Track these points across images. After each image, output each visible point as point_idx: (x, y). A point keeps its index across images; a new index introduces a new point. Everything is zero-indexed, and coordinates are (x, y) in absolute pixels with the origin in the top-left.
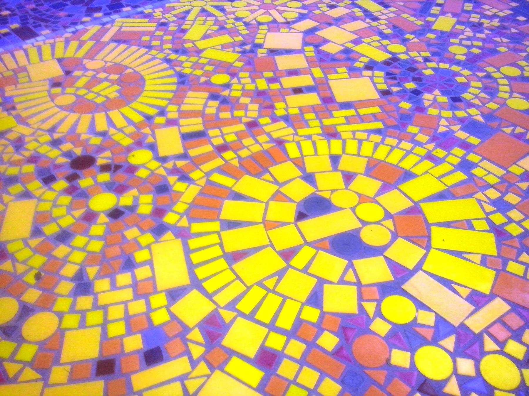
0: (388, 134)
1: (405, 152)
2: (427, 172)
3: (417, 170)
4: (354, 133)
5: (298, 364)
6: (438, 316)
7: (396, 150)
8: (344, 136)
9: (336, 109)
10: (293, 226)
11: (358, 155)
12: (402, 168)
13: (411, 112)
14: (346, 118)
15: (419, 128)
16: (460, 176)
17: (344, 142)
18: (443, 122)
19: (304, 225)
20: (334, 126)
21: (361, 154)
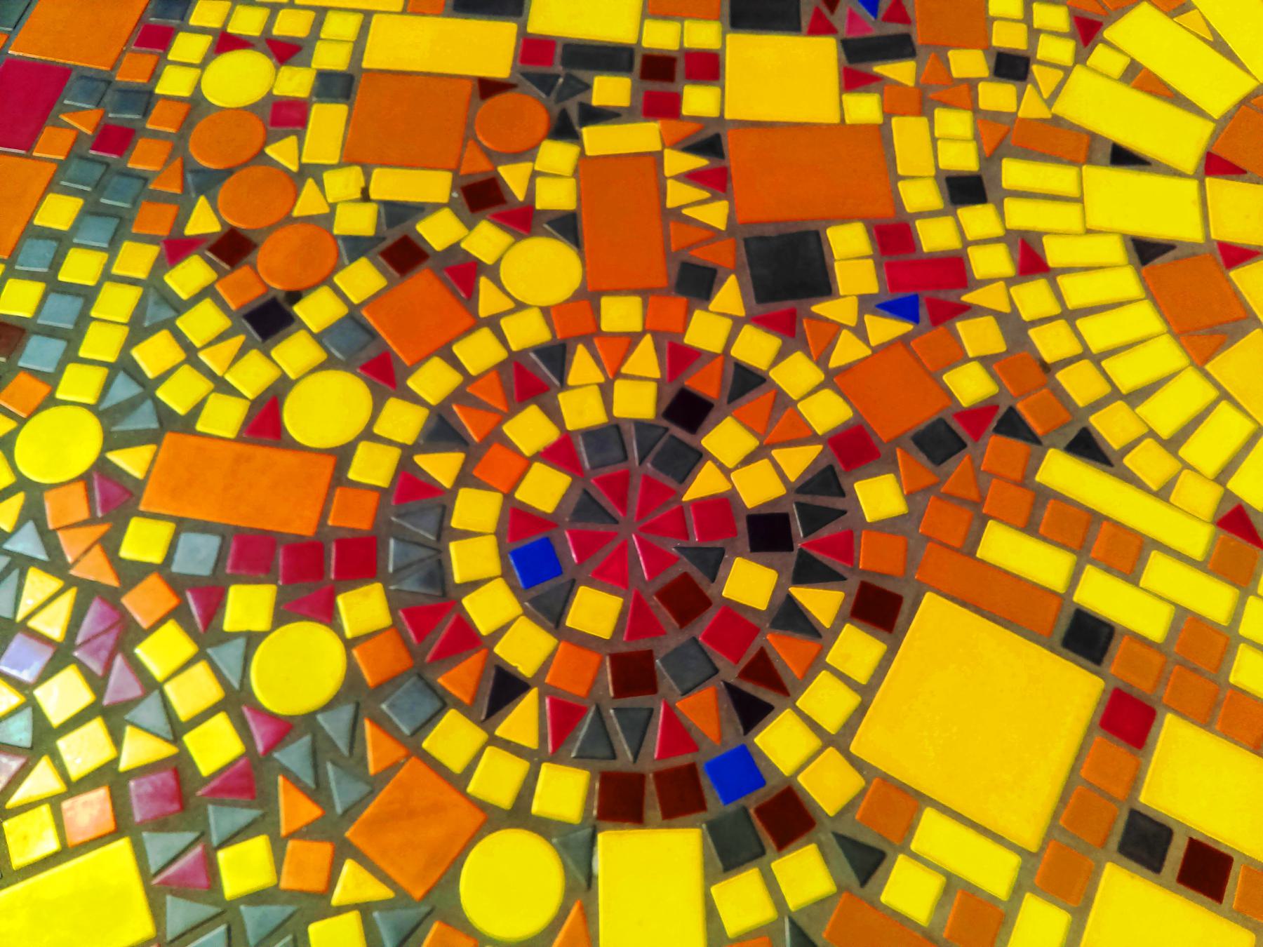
0: (1157, 660)
1: (1080, 323)
2: (1089, 232)
3: (1114, 251)
4: (1163, 494)
5: (574, 197)
6: (545, 311)
7: (1096, 346)
8: (1203, 498)
9: (1136, 647)
10: (1193, 185)
11: (1225, 396)
12: (1143, 280)
13: (895, 462)
14: (1131, 575)
15: (945, 378)
16: (1015, 173)
17: (1224, 475)
18: (847, 351)
19: (1221, 189)
20: (1213, 566)
21: (1212, 394)
